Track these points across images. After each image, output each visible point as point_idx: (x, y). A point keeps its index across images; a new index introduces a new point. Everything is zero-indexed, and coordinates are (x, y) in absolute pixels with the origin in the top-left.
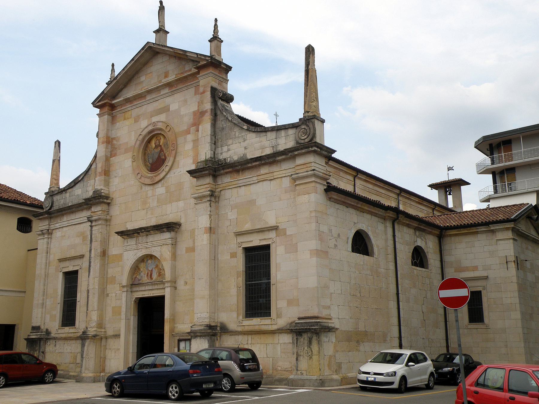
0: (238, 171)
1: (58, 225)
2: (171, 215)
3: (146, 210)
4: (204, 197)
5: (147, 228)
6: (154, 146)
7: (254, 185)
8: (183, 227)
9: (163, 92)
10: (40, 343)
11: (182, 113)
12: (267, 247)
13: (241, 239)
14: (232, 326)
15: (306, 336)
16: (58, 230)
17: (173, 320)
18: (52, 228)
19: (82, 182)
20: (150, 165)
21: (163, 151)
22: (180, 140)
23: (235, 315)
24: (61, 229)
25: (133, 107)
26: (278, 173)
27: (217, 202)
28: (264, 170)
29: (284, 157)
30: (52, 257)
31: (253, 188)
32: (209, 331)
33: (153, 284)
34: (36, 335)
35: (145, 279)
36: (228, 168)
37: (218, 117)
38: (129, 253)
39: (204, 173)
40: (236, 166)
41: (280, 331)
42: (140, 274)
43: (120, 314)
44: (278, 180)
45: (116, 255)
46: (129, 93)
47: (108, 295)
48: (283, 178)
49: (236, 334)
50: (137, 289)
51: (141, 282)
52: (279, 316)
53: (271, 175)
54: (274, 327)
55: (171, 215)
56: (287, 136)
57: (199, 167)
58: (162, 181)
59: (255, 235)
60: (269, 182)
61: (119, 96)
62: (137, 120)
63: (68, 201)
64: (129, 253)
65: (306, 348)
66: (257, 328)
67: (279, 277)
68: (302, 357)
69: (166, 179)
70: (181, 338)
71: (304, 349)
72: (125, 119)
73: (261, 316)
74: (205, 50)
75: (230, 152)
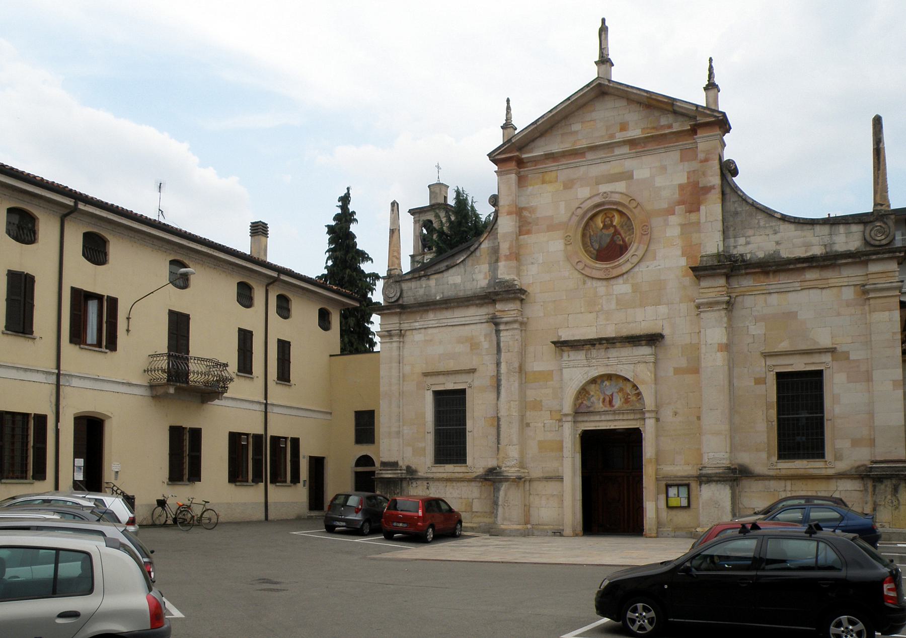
0: (766, 273)
2: (643, 323)
4: (718, 303)
5: (613, 338)
6: (601, 225)
8: (668, 340)
9: (618, 151)
11: (658, 184)
12: (820, 373)
13: (771, 362)
14: (759, 469)
15: (888, 485)
17: (658, 459)
19: (461, 265)
20: (595, 252)
21: (620, 234)
22: (656, 222)
23: (764, 455)
24: (423, 331)
26: (836, 280)
27: (731, 311)
28: (811, 275)
29: (850, 260)
30: (407, 369)
33: (614, 413)
35: (599, 406)
36: (754, 268)
37: (728, 197)
38: (577, 372)
41: (841, 476)
42: (589, 399)
43: (561, 449)
44: (835, 290)
45: (540, 372)
46: (555, 145)
47: (528, 425)
50: (585, 418)
51: (591, 409)
52: (838, 457)
54: (830, 472)
55: (643, 323)
56: (848, 234)
58: (625, 276)
59: (798, 357)
60: (819, 291)
61: (529, 147)
62: (568, 185)
63: (433, 291)
64: (577, 372)
65: (889, 497)
66: (802, 472)
67: (837, 410)
68: (882, 508)
69: (631, 274)
70: (669, 482)
72: (543, 182)
73: (808, 458)
74: (700, 99)
75: (750, 246)
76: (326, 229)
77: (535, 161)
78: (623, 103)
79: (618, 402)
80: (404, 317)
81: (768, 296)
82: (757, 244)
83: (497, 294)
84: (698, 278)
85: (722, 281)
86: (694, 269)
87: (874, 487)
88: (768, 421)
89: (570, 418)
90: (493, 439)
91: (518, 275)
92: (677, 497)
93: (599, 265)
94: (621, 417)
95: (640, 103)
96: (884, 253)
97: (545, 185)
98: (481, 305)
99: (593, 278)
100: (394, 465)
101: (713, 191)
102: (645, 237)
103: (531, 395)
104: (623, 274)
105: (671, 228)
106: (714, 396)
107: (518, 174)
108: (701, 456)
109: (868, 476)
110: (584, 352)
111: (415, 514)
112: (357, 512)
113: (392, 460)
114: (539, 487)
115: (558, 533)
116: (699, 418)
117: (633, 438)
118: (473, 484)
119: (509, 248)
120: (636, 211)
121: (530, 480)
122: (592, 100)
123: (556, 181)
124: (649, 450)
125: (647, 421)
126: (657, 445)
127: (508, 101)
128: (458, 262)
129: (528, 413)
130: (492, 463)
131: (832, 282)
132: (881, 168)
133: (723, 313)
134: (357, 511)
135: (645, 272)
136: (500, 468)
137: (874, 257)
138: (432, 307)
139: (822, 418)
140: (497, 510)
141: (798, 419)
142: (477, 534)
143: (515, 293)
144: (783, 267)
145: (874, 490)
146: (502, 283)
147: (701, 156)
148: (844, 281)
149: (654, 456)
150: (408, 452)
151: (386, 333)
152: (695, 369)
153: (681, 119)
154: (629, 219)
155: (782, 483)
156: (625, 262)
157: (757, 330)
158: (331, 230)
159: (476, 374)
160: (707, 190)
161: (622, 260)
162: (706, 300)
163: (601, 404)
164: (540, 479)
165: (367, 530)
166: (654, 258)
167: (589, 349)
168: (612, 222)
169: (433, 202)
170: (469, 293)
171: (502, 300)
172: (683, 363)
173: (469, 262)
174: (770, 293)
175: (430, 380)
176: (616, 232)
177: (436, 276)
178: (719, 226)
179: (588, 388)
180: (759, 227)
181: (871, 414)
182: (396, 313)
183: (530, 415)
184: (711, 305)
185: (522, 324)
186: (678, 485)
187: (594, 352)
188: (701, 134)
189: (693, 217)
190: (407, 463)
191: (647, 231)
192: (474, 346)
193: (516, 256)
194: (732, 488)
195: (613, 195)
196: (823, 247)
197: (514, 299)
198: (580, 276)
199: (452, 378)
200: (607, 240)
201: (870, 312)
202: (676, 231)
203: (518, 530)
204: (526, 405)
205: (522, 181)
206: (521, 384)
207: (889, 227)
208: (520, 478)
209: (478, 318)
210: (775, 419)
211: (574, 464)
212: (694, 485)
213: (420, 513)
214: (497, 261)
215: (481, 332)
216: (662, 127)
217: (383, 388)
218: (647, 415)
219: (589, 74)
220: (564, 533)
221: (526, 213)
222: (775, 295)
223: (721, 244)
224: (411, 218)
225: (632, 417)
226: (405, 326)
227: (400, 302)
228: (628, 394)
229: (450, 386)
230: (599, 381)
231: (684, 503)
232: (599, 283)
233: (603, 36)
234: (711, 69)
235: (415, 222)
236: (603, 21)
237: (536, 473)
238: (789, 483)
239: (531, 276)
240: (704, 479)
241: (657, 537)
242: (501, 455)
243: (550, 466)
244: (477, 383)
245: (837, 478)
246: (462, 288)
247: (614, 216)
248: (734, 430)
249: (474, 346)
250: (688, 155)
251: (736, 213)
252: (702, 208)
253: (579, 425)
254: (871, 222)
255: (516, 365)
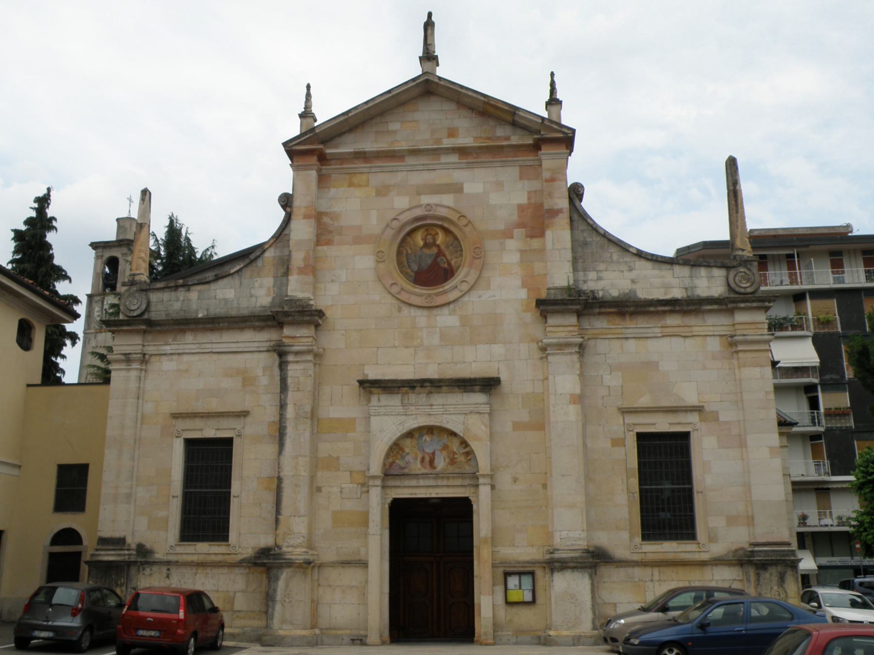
0: (622, 314)
1: (167, 349)
2: (474, 365)
3: (412, 350)
4: (569, 345)
5: (440, 381)
6: (421, 243)
7: (654, 340)
9: (444, 159)
10: (128, 570)
12: (686, 436)
13: (630, 419)
14: (620, 552)
15: (774, 571)
16: (165, 358)
18: (150, 353)
19: (236, 277)
20: (413, 274)
21: (444, 255)
22: (491, 245)
23: (626, 535)
24: (175, 357)
26: (701, 329)
28: (673, 321)
29: (715, 307)
30: (149, 407)
31: (652, 344)
32: (591, 560)
33: (437, 476)
34: (119, 555)
35: (417, 467)
37: (575, 224)
38: (390, 421)
40: (627, 306)
41: (718, 562)
42: (403, 458)
43: (365, 522)
44: (699, 339)
46: (368, 143)
47: (319, 489)
48: (708, 338)
49: (630, 566)
50: (398, 483)
51: (406, 471)
52: (713, 539)
53: (685, 329)
54: (705, 557)
55: (474, 365)
56: (710, 278)
58: (452, 306)
60: (682, 340)
62: (382, 191)
64: (390, 421)
65: (775, 588)
66: (670, 557)
67: (709, 480)
70: (509, 569)
71: (771, 588)
72: (351, 185)
76: (12, 235)
77: (342, 159)
78: (452, 106)
79: (441, 463)
80: (149, 337)
81: (624, 341)
82: (611, 281)
83: (287, 314)
84: (544, 316)
85: (573, 320)
86: (540, 303)
87: (758, 575)
88: (629, 491)
89: (378, 482)
90: (270, 506)
91: (314, 294)
92: (519, 588)
93: (418, 290)
94: (445, 482)
95: (471, 109)
96: (753, 301)
97: (352, 189)
98: (261, 329)
99: (410, 305)
100: (120, 542)
101: (561, 215)
102: (477, 261)
103: (325, 448)
104: (449, 304)
105: (509, 255)
106: (566, 462)
107: (319, 171)
108: (550, 535)
109: (750, 563)
110: (399, 396)
111: (174, 616)
112: (74, 615)
113: (117, 535)
114: (333, 575)
115: (360, 641)
116: (545, 486)
117: (461, 510)
118: (237, 570)
119: (305, 259)
120: (467, 230)
121: (321, 566)
122: (415, 98)
123: (367, 185)
124: (482, 526)
125: (481, 488)
126: (493, 521)
127: (308, 87)
128: (232, 271)
129: (319, 474)
130: (266, 541)
131: (696, 330)
132: (740, 211)
133: (575, 357)
134: (75, 612)
135: (477, 303)
136: (280, 548)
137: (742, 305)
138: (192, 326)
139: (691, 491)
140: (273, 609)
141: (661, 491)
142: (242, 645)
143: (312, 315)
144: (642, 309)
145: (758, 580)
146: (292, 301)
147: (546, 175)
148: (709, 330)
149: (490, 535)
150: (142, 524)
151: (123, 357)
152: (539, 423)
153: (519, 131)
154: (456, 238)
155: (648, 571)
156: (451, 289)
157: (613, 380)
158: (18, 235)
159: (249, 419)
160: (554, 213)
161: (448, 286)
162: (555, 341)
163: (419, 465)
164: (333, 565)
165: (85, 644)
166: (488, 287)
167: (407, 393)
168: (434, 240)
169: (121, 237)
170: (245, 312)
171: (292, 324)
172: (524, 416)
173: (247, 273)
174: (627, 338)
175: (181, 424)
176: (440, 253)
177: (199, 287)
178: (569, 255)
179: (401, 443)
180: (612, 261)
181: (748, 487)
182: (138, 332)
183: (322, 476)
184: (561, 346)
185: (317, 356)
186: (520, 574)
187: (412, 397)
188: (545, 150)
189: (536, 243)
190: (138, 539)
191: (479, 253)
192: (248, 381)
193: (312, 269)
194: (591, 576)
195: (439, 209)
196: (684, 290)
197: (308, 323)
198: (394, 301)
199: (212, 423)
200: (430, 260)
201: (739, 367)
202: (515, 258)
203: (304, 637)
204: (319, 464)
205: (323, 180)
206: (312, 434)
207: (753, 274)
208: (309, 563)
209: (256, 344)
210: (638, 490)
211: (382, 545)
212: (539, 573)
213: (181, 615)
214: (287, 273)
215: (261, 365)
216: (498, 138)
217: (112, 431)
218: (481, 481)
219: (415, 70)
220: (369, 640)
221: (326, 220)
222: (632, 342)
223: (571, 275)
224: (92, 253)
225: (459, 482)
226: (150, 349)
227: (146, 316)
228: (454, 453)
229: (210, 433)
230: (416, 435)
231: (528, 597)
232: (418, 312)
233: (429, 31)
234: (553, 84)
235: (97, 257)
236: (430, 15)
237: (328, 554)
238: (656, 571)
239: (329, 297)
240: (556, 565)
241: (494, 644)
242: (282, 529)
243: (349, 546)
244: (248, 431)
245: (713, 565)
246: (235, 304)
247: (437, 234)
248: (590, 502)
249: (248, 381)
250: (529, 172)
251: (585, 244)
252: (549, 233)
253: (389, 491)
254: (734, 267)
255: (308, 408)
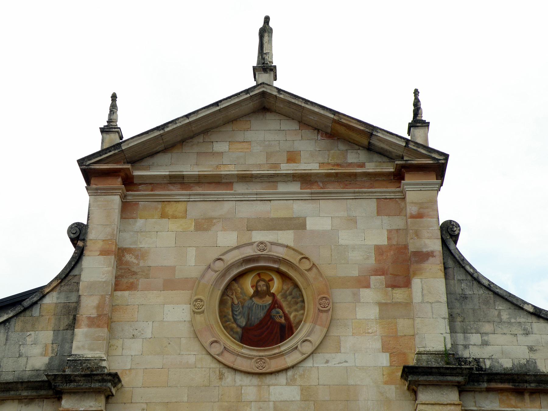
6: (251, 291)
9: (282, 188)
20: (239, 330)
21: (281, 307)
25: (193, 198)
39: (449, 378)
40: (526, 382)
46: (187, 165)
57: (420, 365)
58: (290, 373)
62: (203, 225)
69: (300, 370)
72: (163, 216)
